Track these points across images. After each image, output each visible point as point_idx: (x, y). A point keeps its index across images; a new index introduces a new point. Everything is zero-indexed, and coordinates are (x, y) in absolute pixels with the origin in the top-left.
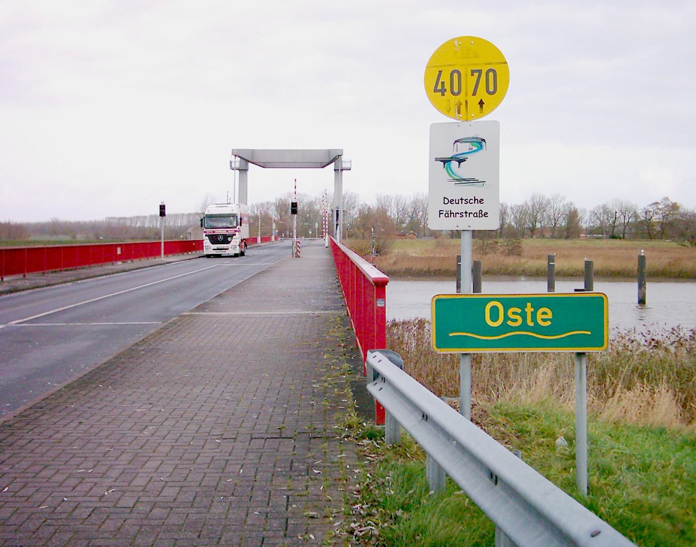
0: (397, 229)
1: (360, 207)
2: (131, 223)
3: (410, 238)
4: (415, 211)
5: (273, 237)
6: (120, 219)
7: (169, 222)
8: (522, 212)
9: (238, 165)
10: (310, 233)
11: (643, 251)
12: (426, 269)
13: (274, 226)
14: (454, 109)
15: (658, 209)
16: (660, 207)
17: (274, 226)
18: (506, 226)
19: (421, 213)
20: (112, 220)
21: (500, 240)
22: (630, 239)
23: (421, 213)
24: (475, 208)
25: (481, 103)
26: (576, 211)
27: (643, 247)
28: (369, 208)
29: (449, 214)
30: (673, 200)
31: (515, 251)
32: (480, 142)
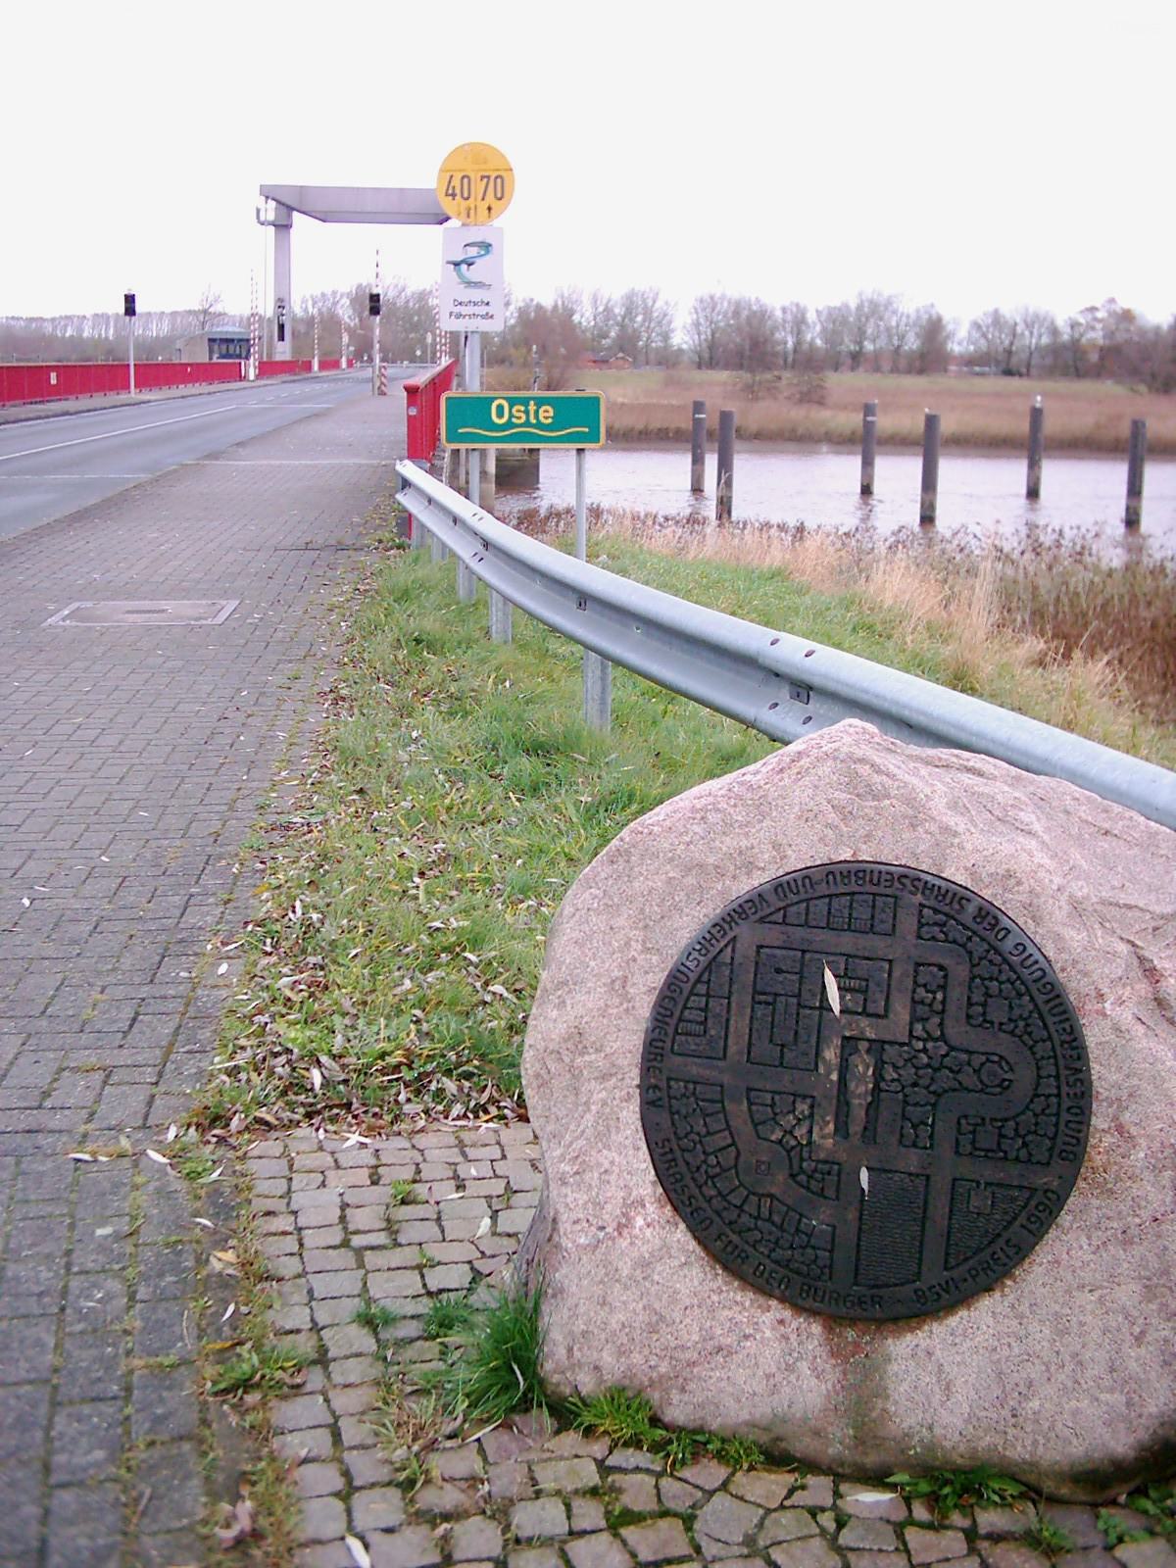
0: (593, 350)
1: (522, 304)
2: (55, 328)
3: (617, 368)
4: (630, 312)
5: (344, 363)
6: (31, 320)
7: (137, 327)
8: (836, 320)
9: (271, 217)
10: (418, 353)
11: (1039, 398)
12: (640, 426)
13: (346, 339)
14: (464, 214)
15: (1096, 319)
16: (1100, 315)
17: (346, 339)
18: (805, 347)
19: (639, 318)
20: (12, 322)
21: (787, 375)
22: (1040, 377)
23: (639, 318)
24: (483, 310)
25: (489, 209)
26: (939, 320)
27: (1037, 393)
28: (539, 307)
29: (459, 316)
30: (1124, 303)
31: (813, 396)
32: (486, 247)
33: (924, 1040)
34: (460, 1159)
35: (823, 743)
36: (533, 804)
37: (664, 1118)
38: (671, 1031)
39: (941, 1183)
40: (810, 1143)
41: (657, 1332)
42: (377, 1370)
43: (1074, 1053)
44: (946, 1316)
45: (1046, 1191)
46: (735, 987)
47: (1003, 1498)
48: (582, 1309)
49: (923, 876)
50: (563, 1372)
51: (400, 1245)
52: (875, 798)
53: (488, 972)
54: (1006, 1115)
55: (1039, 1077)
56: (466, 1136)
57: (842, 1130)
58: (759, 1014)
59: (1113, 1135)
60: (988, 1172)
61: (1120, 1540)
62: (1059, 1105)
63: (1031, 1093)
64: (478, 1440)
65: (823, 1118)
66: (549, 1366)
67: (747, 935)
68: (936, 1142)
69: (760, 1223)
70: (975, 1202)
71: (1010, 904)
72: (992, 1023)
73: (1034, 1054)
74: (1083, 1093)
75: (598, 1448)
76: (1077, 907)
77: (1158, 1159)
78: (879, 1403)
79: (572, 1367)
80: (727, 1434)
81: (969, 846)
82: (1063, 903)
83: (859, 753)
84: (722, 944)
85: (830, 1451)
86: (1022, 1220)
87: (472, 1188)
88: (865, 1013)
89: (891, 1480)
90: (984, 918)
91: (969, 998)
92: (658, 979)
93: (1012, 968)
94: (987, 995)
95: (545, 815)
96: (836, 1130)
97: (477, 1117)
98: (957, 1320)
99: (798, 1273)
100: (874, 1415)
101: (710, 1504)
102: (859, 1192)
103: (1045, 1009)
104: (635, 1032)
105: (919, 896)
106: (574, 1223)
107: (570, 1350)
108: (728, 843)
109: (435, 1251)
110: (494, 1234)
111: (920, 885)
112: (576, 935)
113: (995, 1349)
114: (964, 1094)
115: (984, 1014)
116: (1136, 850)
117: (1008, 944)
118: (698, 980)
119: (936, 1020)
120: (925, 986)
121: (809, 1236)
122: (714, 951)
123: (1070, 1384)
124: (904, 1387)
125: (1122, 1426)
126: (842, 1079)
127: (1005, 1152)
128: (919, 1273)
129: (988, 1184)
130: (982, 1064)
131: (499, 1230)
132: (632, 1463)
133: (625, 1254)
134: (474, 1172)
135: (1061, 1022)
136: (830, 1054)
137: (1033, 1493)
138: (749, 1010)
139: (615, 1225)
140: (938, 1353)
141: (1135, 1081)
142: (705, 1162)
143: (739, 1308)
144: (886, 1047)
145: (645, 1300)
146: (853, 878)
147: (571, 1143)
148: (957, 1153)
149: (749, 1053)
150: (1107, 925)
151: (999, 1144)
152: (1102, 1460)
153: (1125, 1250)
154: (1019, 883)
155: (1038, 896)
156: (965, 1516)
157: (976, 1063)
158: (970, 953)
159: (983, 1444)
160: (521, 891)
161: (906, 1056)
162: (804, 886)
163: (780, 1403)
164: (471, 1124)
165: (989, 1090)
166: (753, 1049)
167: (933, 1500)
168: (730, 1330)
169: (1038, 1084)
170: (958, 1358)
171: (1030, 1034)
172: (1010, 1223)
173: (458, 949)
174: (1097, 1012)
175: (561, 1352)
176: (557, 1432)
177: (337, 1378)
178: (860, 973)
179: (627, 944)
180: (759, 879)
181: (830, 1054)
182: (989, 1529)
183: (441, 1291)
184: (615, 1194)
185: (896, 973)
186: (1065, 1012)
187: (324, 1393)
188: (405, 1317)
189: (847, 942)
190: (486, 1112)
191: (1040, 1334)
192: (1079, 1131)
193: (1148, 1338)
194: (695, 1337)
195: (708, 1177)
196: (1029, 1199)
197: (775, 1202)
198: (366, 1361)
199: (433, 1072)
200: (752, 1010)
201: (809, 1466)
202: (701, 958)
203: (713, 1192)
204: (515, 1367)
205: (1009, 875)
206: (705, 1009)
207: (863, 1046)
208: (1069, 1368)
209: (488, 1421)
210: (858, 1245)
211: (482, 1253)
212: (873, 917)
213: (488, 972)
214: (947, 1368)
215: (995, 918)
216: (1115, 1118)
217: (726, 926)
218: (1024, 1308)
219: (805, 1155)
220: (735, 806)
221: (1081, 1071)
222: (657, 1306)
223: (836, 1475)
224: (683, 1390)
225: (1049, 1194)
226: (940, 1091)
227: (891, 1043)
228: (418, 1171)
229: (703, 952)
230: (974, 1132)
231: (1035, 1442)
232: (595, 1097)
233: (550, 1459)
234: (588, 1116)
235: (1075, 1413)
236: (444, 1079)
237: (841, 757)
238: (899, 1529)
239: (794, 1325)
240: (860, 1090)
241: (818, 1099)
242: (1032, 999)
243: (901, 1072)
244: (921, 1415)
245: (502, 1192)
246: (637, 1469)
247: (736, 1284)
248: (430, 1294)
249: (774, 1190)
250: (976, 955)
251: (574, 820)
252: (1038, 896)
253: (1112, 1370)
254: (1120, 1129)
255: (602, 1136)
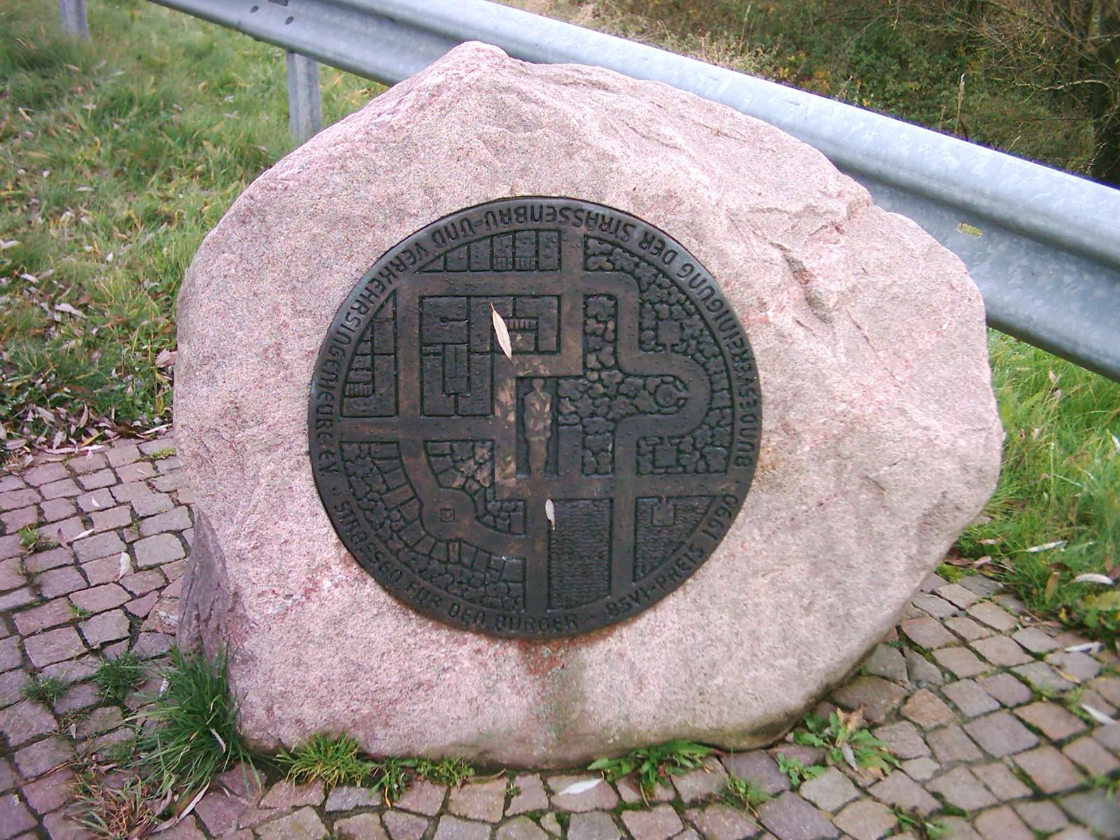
33: (599, 371)
34: (77, 491)
35: (462, 73)
36: (43, 117)
37: (340, 482)
38: (337, 394)
39: (624, 504)
40: (493, 484)
41: (356, 680)
42: (65, 754)
43: (746, 365)
44: (634, 621)
45: (725, 496)
46: (400, 342)
47: (693, 761)
48: (277, 673)
49: (586, 206)
50: (264, 730)
51: (48, 600)
52: (527, 128)
53: (49, 291)
54: (681, 432)
55: (713, 391)
56: (76, 463)
57: (524, 465)
58: (429, 365)
59: (780, 435)
60: (669, 487)
61: (802, 779)
62: (733, 414)
63: (705, 409)
64: (193, 812)
65: (504, 459)
66: (248, 726)
67: (405, 285)
68: (617, 466)
69: (450, 566)
70: (659, 517)
71: (672, 224)
72: (664, 346)
73: (706, 370)
74: (755, 402)
75: (314, 795)
76: (734, 220)
77: (821, 450)
78: (579, 706)
79: (273, 724)
80: (436, 755)
81: (628, 171)
82: (723, 218)
83: (503, 82)
84: (382, 299)
85: (535, 753)
86: (703, 526)
87: (100, 522)
88: (537, 351)
89: (593, 767)
90: (650, 243)
91: (640, 324)
92: (315, 341)
93: (682, 291)
94: (658, 318)
95: (58, 127)
96: (518, 468)
97: (80, 441)
98: (645, 622)
99: (492, 606)
100: (575, 716)
101: (439, 832)
102: (546, 524)
103: (715, 325)
104: (296, 399)
105: (583, 227)
106: (259, 595)
107: (269, 710)
108: (374, 192)
109: (85, 601)
110: (137, 570)
111: (583, 216)
112: (215, 305)
113: (681, 641)
114: (642, 418)
115: (656, 337)
116: (746, 148)
117: (676, 267)
118: (361, 340)
119: (609, 349)
120: (595, 317)
121: (501, 570)
122: (374, 308)
123: (748, 658)
124: (601, 688)
125: (795, 684)
126: (521, 420)
127: (684, 467)
128: (610, 587)
129: (669, 498)
130: (657, 386)
131: (140, 564)
132: (350, 803)
133: (315, 616)
134: (96, 504)
135: (731, 337)
136: (506, 397)
137: (719, 750)
138: (418, 364)
139: (302, 591)
140: (630, 654)
141: (799, 382)
142: (388, 517)
143: (435, 646)
144: (561, 381)
145: (340, 654)
146: (514, 216)
147: (244, 519)
148: (638, 473)
149: (422, 405)
150: (758, 232)
151: (678, 460)
152: (778, 715)
153: (793, 535)
154: (680, 203)
155: (699, 214)
156: (665, 787)
157: (651, 387)
158: (638, 279)
159: (674, 722)
160: (57, 204)
161: (581, 389)
162: (463, 229)
163: (484, 722)
164: (76, 450)
165: (665, 410)
166: (427, 402)
167: (636, 779)
168: (429, 667)
169: (712, 399)
170: (649, 655)
171: (701, 352)
172: (692, 531)
173: (16, 273)
174: (761, 321)
175: (260, 713)
176: (268, 785)
177: (28, 771)
178: (530, 312)
179: (276, 309)
180: (411, 227)
181: (506, 397)
182: (692, 796)
183: (104, 645)
184: (298, 564)
185: (566, 308)
186: (735, 326)
187: (18, 791)
188: (74, 683)
189: (513, 282)
190: (88, 435)
191: (720, 620)
192: (754, 437)
193: (816, 607)
194: (395, 678)
195: (393, 531)
196: (709, 506)
197: (463, 544)
198: (52, 742)
199: (26, 404)
200: (421, 362)
201: (515, 769)
202: (361, 317)
203: (400, 545)
204: (214, 731)
205: (670, 195)
206: (372, 368)
207: (538, 384)
208: (746, 645)
209: (196, 787)
210: (549, 572)
211: (130, 593)
212: (537, 252)
213: (49, 291)
214: (638, 665)
215: (663, 243)
216: (782, 418)
217: (384, 280)
218: (705, 601)
219: (489, 497)
220: (376, 150)
221: (752, 381)
222: (353, 657)
223: (541, 771)
224: (387, 725)
225: (728, 499)
226: (618, 417)
227: (566, 377)
228: (41, 512)
229: (363, 309)
230: (653, 452)
231: (720, 713)
232: (263, 470)
233: (270, 819)
234: (258, 490)
235: (754, 681)
236: (40, 409)
237: (486, 87)
238: (617, 812)
239: (491, 651)
240: (539, 426)
241: (498, 441)
242: (702, 317)
243: (579, 404)
244: (618, 709)
245: (130, 521)
246: (358, 809)
247: (430, 624)
248: (95, 652)
249: (460, 535)
250: (644, 280)
251: (85, 127)
252: (699, 214)
253: (785, 639)
254: (786, 427)
255: (277, 509)
